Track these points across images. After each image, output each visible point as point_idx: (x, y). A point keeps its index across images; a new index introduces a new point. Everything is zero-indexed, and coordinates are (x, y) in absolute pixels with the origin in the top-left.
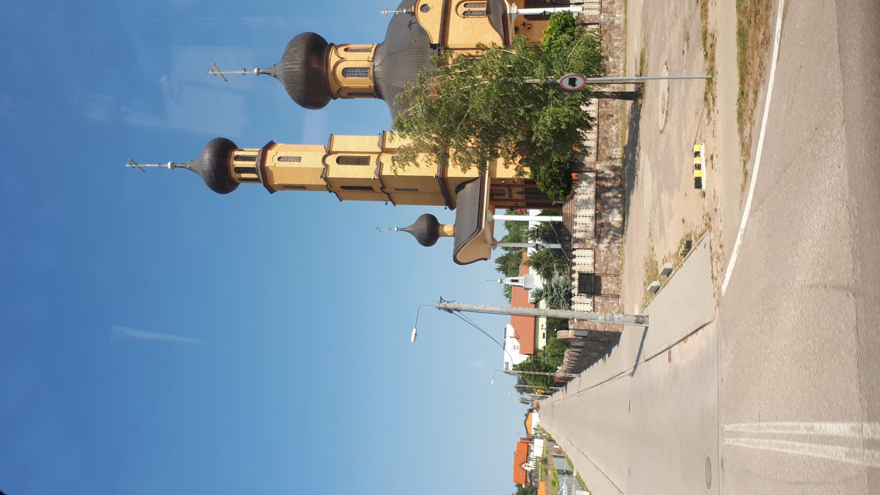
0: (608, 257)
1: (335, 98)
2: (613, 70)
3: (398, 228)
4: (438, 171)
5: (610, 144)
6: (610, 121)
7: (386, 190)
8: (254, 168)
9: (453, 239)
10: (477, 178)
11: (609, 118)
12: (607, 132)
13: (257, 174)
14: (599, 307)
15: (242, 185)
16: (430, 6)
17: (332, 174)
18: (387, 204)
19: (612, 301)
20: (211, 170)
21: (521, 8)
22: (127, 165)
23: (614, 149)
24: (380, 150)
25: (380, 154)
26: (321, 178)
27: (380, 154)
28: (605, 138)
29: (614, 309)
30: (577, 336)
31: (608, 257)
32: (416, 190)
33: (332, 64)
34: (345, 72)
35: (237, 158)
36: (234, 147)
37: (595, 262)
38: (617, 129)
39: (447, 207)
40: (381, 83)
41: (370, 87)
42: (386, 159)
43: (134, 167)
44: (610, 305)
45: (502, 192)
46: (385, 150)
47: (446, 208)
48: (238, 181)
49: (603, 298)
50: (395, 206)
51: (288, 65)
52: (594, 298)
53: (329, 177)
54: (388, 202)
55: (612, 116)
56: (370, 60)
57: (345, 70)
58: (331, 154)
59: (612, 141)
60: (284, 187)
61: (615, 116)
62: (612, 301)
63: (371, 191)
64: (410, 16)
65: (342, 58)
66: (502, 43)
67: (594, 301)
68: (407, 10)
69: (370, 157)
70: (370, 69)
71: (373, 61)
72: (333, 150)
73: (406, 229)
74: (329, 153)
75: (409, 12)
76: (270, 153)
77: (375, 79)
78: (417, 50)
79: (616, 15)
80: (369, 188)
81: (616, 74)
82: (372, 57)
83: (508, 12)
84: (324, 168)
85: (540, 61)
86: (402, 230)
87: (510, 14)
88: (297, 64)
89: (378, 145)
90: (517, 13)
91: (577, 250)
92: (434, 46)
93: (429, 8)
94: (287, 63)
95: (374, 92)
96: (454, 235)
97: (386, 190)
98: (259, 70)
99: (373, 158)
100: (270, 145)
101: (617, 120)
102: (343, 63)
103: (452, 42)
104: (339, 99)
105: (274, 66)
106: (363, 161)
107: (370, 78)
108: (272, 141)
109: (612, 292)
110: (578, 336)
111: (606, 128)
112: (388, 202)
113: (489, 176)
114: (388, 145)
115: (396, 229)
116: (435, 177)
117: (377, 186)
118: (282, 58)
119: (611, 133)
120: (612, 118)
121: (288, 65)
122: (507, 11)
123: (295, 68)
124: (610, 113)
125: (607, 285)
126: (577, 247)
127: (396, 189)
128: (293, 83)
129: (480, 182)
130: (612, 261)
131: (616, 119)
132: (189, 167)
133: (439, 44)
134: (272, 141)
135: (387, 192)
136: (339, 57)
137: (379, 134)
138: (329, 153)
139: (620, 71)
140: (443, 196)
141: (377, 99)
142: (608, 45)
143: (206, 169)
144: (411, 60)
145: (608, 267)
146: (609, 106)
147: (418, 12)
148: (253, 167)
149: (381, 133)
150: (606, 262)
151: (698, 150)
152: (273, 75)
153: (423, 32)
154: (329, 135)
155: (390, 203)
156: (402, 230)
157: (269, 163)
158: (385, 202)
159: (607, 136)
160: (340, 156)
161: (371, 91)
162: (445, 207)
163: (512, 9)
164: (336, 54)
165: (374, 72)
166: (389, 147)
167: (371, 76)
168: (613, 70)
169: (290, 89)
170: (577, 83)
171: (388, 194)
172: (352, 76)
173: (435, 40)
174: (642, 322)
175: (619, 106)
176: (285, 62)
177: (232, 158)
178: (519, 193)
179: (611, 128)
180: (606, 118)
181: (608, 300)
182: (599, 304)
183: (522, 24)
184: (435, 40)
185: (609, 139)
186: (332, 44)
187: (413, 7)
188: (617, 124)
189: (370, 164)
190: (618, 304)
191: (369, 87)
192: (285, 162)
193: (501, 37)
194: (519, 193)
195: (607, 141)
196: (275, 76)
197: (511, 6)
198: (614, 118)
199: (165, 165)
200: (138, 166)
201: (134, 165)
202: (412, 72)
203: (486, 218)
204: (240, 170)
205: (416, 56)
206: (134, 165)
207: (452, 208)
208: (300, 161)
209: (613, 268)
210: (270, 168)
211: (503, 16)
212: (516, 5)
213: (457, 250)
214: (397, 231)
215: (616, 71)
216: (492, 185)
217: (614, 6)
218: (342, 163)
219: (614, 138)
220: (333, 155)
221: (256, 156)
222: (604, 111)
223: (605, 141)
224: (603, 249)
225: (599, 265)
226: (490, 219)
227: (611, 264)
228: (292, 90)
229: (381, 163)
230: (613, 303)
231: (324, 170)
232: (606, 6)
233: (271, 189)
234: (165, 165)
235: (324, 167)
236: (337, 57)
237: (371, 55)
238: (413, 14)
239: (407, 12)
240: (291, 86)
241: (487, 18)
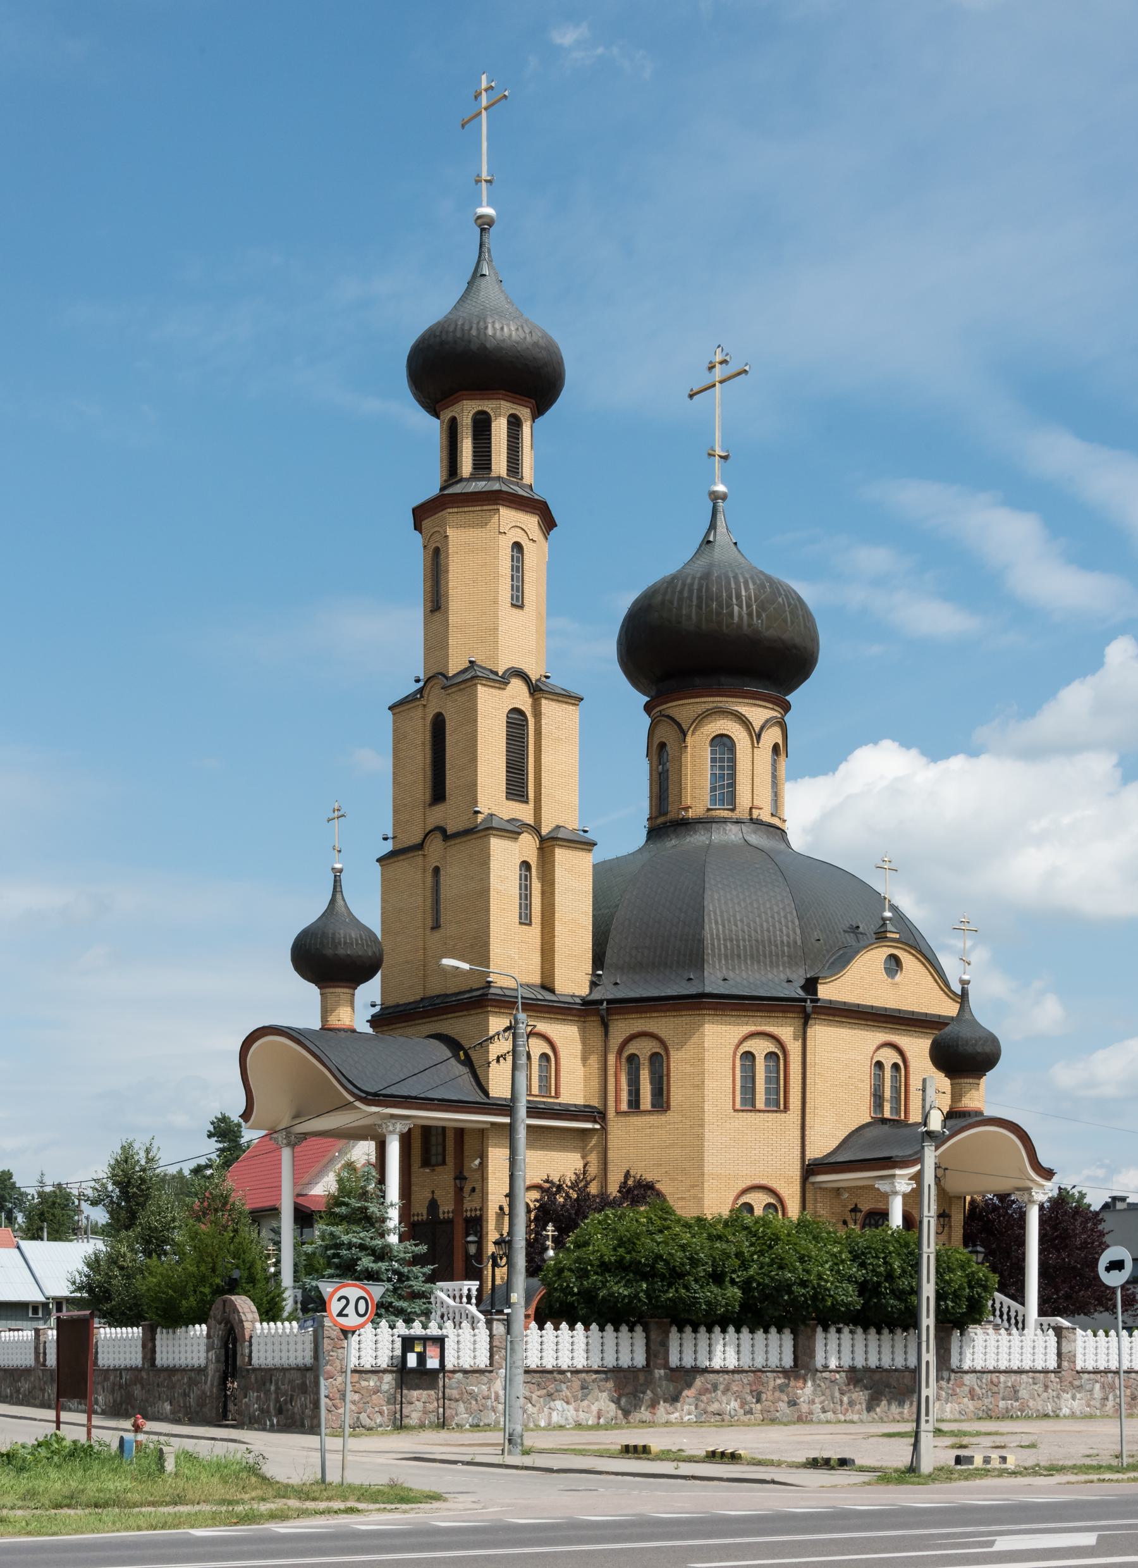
0: (476, 1400)
1: (648, 708)
2: (845, 1399)
3: (341, 871)
4: (501, 988)
5: (704, 1398)
6: (749, 1398)
7: (435, 846)
8: (490, 469)
9: (316, 1025)
10: (486, 1093)
11: (754, 1394)
12: (727, 1390)
13: (473, 477)
14: (372, 1384)
15: (431, 428)
16: (898, 978)
17: (484, 694)
18: (385, 839)
19: (386, 1412)
20: (488, 345)
21: (904, 1204)
22: (484, 77)
23: (693, 1407)
24: (544, 831)
25: (535, 829)
26: (471, 662)
27: (535, 829)
28: (715, 1387)
29: (369, 1417)
30: (250, 1342)
31: (476, 1400)
32: (436, 926)
33: (744, 710)
34: (723, 742)
35: (515, 424)
36: (539, 410)
37: (465, 1372)
38: (733, 1413)
39: (378, 1009)
40: (698, 839)
41: (686, 809)
42: (527, 847)
43: (477, 96)
44: (377, 1409)
45: (433, 1160)
46: (548, 844)
47: (373, 1005)
48: (447, 415)
49: (392, 1391)
50: (378, 860)
51: (747, 589)
52: (391, 1372)
53: (479, 687)
54: (390, 842)
55: (758, 1401)
56: (755, 813)
57: (725, 739)
58: (531, 694)
59: (710, 1402)
60: (437, 551)
61: (759, 1406)
62: (386, 1412)
63: (428, 797)
64: (873, 928)
65: (759, 736)
66: (817, 1156)
67: (384, 1371)
68: (890, 919)
69: (527, 802)
70: (733, 810)
71: (751, 819)
72: (544, 701)
73: (339, 896)
74: (536, 690)
75: (884, 924)
76: (531, 522)
77: (706, 822)
78: (799, 942)
79: (949, 1404)
80: (438, 794)
81: (839, 1408)
82: (761, 817)
83: (898, 1172)
84: (496, 673)
85: (184, 1302)
86: (337, 882)
87: (894, 1176)
88: (750, 614)
89: (558, 827)
90: (895, 1193)
91: (488, 1332)
92: (811, 985)
93: (893, 977)
94: (751, 586)
95: (670, 817)
96: (325, 1029)
97: (435, 846)
98: (724, 497)
99: (523, 812)
100: (548, 523)
101: (750, 1412)
102: (748, 738)
103: (822, 1034)
104: (646, 721)
105: (735, 544)
106: (516, 788)
107: (709, 810)
108: (556, 526)
109: (405, 1411)
110: (251, 1345)
111: (735, 1389)
112: (390, 842)
113: (493, 1124)
114: (562, 856)
115: (338, 866)
116: (489, 979)
117: (450, 816)
118: (761, 572)
119: (724, 1399)
120: (754, 1400)
121: (747, 589)
122: (901, 1168)
123: (741, 607)
124: (764, 1396)
125: (419, 1400)
126: (495, 1332)
127: (436, 871)
128: (699, 598)
129: (479, 1100)
130: (469, 1411)
131: (751, 1409)
132: (486, 271)
133: (818, 1000)
134: (556, 526)
135: (428, 842)
136: (762, 728)
137: (585, 831)
138: (536, 690)
139: (845, 1415)
140: (418, 998)
141: (646, 823)
142: (894, 1388)
143: (490, 332)
144: (774, 926)
145: (457, 1401)
146: (777, 1394)
147: (885, 949)
148: (493, 467)
149: (585, 834)
150: (465, 1396)
151: (1008, 1460)
152: (711, 539)
153: (841, 960)
154: (581, 694)
155: (388, 846)
156: (337, 882)
157: (508, 516)
158: (390, 835)
159: (719, 1392)
160: (526, 720)
161: (672, 808)
162: (379, 1002)
163: (903, 1182)
164: (767, 721)
165: (724, 821)
166: (557, 856)
167: (714, 813)
168: (845, 1399)
169: (684, 584)
170: (1115, 1273)
171: (420, 846)
172: (713, 760)
173: (825, 992)
174: (513, 1441)
175: (778, 1414)
176: (752, 578)
177: (515, 406)
178: (433, 1205)
179: (736, 1400)
180: (754, 1388)
181: (388, 1403)
182: (378, 1384)
183: (856, 1205)
184: (825, 992)
185: (713, 1395)
186: (786, 707)
187: (897, 936)
188: (742, 1411)
189: (511, 803)
190: (381, 1426)
191: (684, 805)
192: (509, 564)
193: (829, 1155)
194: (433, 1205)
195: (710, 1393)
196: (709, 542)
197: (910, 1179)
198: (753, 1406)
199: (484, 203)
200: (484, 113)
201: (484, 100)
202: (746, 928)
203: (392, 1116)
204: (482, 427)
205: (785, 938)
206: (484, 100)
207: (375, 1022)
208: (513, 605)
209: (454, 1412)
210: (495, 519)
211: (890, 1158)
212: (913, 1189)
213: (302, 1039)
214: (333, 869)
215: (845, 1406)
216: (460, 1133)
217: (966, 1400)
218: (510, 724)
219: (715, 1407)
220: (529, 701)
221: (522, 479)
222: (767, 1383)
223: (709, 1386)
224: (492, 1390)
225: (459, 1382)
226: (391, 1128)
227: (461, 1407)
228: (681, 592)
229: (519, 834)
230: (381, 1413)
231: (492, 672)
232: (967, 1383)
233: (422, 514)
234: (484, 203)
235: (500, 674)
236: (761, 723)
237: (765, 816)
238: (881, 936)
239: (884, 919)
240: (691, 591)
241: (869, 1120)
